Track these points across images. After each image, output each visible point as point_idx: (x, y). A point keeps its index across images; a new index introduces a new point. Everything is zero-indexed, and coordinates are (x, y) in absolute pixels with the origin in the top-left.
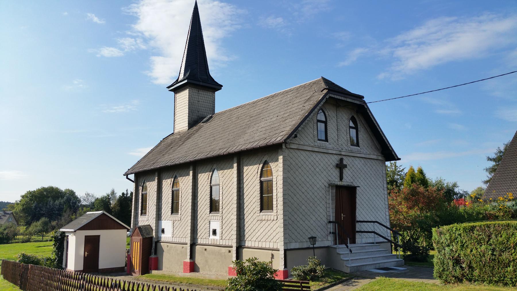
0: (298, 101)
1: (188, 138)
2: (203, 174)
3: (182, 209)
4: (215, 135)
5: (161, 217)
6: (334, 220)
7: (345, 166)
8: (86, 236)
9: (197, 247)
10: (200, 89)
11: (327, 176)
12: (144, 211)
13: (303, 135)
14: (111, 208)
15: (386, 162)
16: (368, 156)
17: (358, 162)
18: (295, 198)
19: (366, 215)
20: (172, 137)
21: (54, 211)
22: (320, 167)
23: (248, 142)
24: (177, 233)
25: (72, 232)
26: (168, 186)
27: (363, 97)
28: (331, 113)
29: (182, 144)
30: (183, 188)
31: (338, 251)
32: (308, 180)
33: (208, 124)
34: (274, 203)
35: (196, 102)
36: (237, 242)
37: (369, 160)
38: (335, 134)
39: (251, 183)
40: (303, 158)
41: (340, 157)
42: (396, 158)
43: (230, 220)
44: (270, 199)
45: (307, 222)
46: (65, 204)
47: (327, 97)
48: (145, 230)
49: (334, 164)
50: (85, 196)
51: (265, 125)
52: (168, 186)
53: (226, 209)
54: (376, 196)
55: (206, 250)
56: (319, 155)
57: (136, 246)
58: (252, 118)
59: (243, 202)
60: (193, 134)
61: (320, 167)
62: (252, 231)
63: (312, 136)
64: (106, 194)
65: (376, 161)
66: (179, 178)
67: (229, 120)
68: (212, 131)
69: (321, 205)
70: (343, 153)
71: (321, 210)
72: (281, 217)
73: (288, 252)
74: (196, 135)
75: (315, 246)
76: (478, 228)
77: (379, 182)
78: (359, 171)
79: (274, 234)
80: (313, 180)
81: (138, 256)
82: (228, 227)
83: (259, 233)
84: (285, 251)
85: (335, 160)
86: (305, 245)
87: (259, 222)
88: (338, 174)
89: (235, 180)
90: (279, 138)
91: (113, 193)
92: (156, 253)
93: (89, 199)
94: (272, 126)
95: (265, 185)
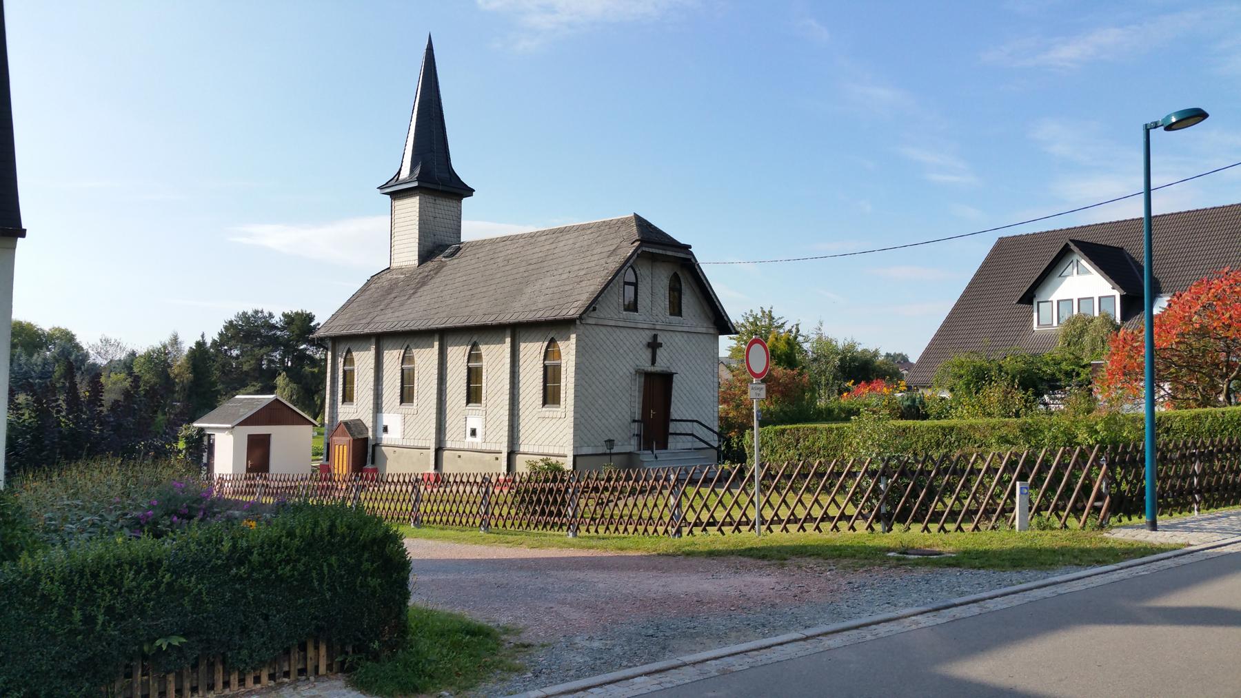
0: (599, 250)
1: (423, 283)
2: (457, 348)
3: (420, 397)
4: (471, 287)
5: (382, 408)
6: (640, 419)
7: (661, 345)
8: (249, 436)
9: (446, 454)
10: (438, 196)
11: (634, 359)
12: (348, 397)
13: (604, 305)
14: (172, 375)
15: (720, 337)
16: (693, 330)
17: (678, 340)
18: (590, 390)
19: (685, 412)
20: (389, 276)
21: (31, 377)
22: (625, 348)
23: (527, 309)
24: (411, 433)
25: (227, 428)
26: (394, 360)
27: (690, 247)
28: (644, 271)
29: (413, 294)
30: (420, 366)
31: (641, 458)
32: (608, 365)
33: (456, 261)
34: (563, 395)
35: (432, 218)
36: (508, 447)
37: (695, 335)
38: (648, 301)
39: (530, 367)
40: (602, 336)
41: (654, 332)
42: (733, 331)
43: (498, 416)
44: (557, 391)
45: (604, 421)
46: (58, 362)
47: (639, 252)
48: (353, 427)
49: (645, 342)
50: (100, 344)
51: (552, 284)
52: (394, 360)
53: (492, 401)
54: (701, 384)
55: (460, 456)
56: (625, 332)
57: (341, 452)
58: (531, 267)
59: (518, 392)
60: (429, 277)
61: (625, 348)
62: (530, 431)
63: (615, 304)
64: (161, 342)
65: (705, 335)
66: (414, 350)
67: (492, 261)
68: (464, 278)
69: (624, 399)
70: (658, 327)
71: (624, 405)
72: (571, 414)
73: (578, 458)
74: (437, 280)
75: (613, 451)
76: (788, 431)
77: (707, 366)
78: (680, 351)
79: (561, 436)
80: (615, 366)
81: (345, 465)
82: (495, 426)
83: (540, 435)
84: (575, 457)
85: (646, 337)
86: (600, 451)
87: (540, 420)
88: (650, 356)
89: (508, 360)
90: (572, 312)
91: (175, 341)
92: (373, 462)
93: (110, 352)
94: (562, 288)
95: (550, 371)
